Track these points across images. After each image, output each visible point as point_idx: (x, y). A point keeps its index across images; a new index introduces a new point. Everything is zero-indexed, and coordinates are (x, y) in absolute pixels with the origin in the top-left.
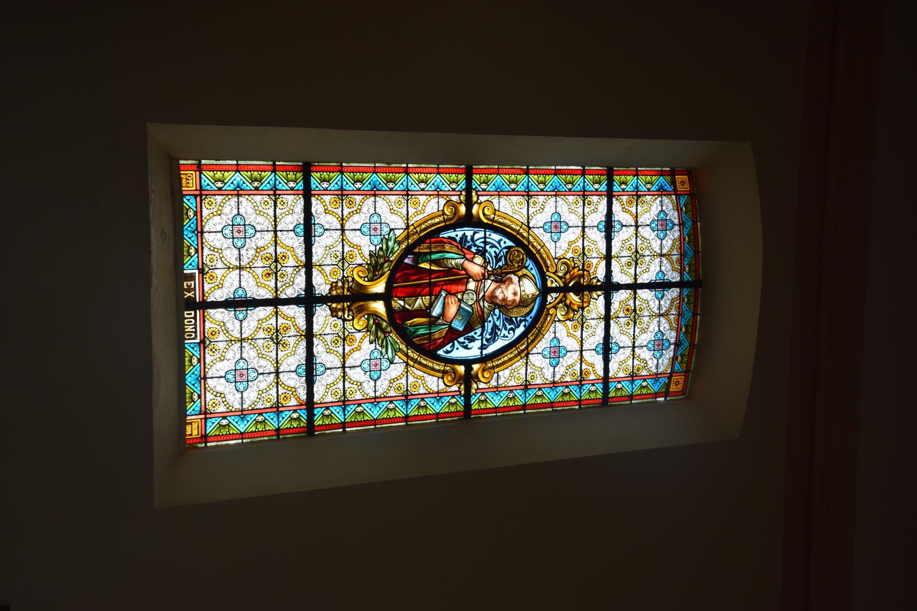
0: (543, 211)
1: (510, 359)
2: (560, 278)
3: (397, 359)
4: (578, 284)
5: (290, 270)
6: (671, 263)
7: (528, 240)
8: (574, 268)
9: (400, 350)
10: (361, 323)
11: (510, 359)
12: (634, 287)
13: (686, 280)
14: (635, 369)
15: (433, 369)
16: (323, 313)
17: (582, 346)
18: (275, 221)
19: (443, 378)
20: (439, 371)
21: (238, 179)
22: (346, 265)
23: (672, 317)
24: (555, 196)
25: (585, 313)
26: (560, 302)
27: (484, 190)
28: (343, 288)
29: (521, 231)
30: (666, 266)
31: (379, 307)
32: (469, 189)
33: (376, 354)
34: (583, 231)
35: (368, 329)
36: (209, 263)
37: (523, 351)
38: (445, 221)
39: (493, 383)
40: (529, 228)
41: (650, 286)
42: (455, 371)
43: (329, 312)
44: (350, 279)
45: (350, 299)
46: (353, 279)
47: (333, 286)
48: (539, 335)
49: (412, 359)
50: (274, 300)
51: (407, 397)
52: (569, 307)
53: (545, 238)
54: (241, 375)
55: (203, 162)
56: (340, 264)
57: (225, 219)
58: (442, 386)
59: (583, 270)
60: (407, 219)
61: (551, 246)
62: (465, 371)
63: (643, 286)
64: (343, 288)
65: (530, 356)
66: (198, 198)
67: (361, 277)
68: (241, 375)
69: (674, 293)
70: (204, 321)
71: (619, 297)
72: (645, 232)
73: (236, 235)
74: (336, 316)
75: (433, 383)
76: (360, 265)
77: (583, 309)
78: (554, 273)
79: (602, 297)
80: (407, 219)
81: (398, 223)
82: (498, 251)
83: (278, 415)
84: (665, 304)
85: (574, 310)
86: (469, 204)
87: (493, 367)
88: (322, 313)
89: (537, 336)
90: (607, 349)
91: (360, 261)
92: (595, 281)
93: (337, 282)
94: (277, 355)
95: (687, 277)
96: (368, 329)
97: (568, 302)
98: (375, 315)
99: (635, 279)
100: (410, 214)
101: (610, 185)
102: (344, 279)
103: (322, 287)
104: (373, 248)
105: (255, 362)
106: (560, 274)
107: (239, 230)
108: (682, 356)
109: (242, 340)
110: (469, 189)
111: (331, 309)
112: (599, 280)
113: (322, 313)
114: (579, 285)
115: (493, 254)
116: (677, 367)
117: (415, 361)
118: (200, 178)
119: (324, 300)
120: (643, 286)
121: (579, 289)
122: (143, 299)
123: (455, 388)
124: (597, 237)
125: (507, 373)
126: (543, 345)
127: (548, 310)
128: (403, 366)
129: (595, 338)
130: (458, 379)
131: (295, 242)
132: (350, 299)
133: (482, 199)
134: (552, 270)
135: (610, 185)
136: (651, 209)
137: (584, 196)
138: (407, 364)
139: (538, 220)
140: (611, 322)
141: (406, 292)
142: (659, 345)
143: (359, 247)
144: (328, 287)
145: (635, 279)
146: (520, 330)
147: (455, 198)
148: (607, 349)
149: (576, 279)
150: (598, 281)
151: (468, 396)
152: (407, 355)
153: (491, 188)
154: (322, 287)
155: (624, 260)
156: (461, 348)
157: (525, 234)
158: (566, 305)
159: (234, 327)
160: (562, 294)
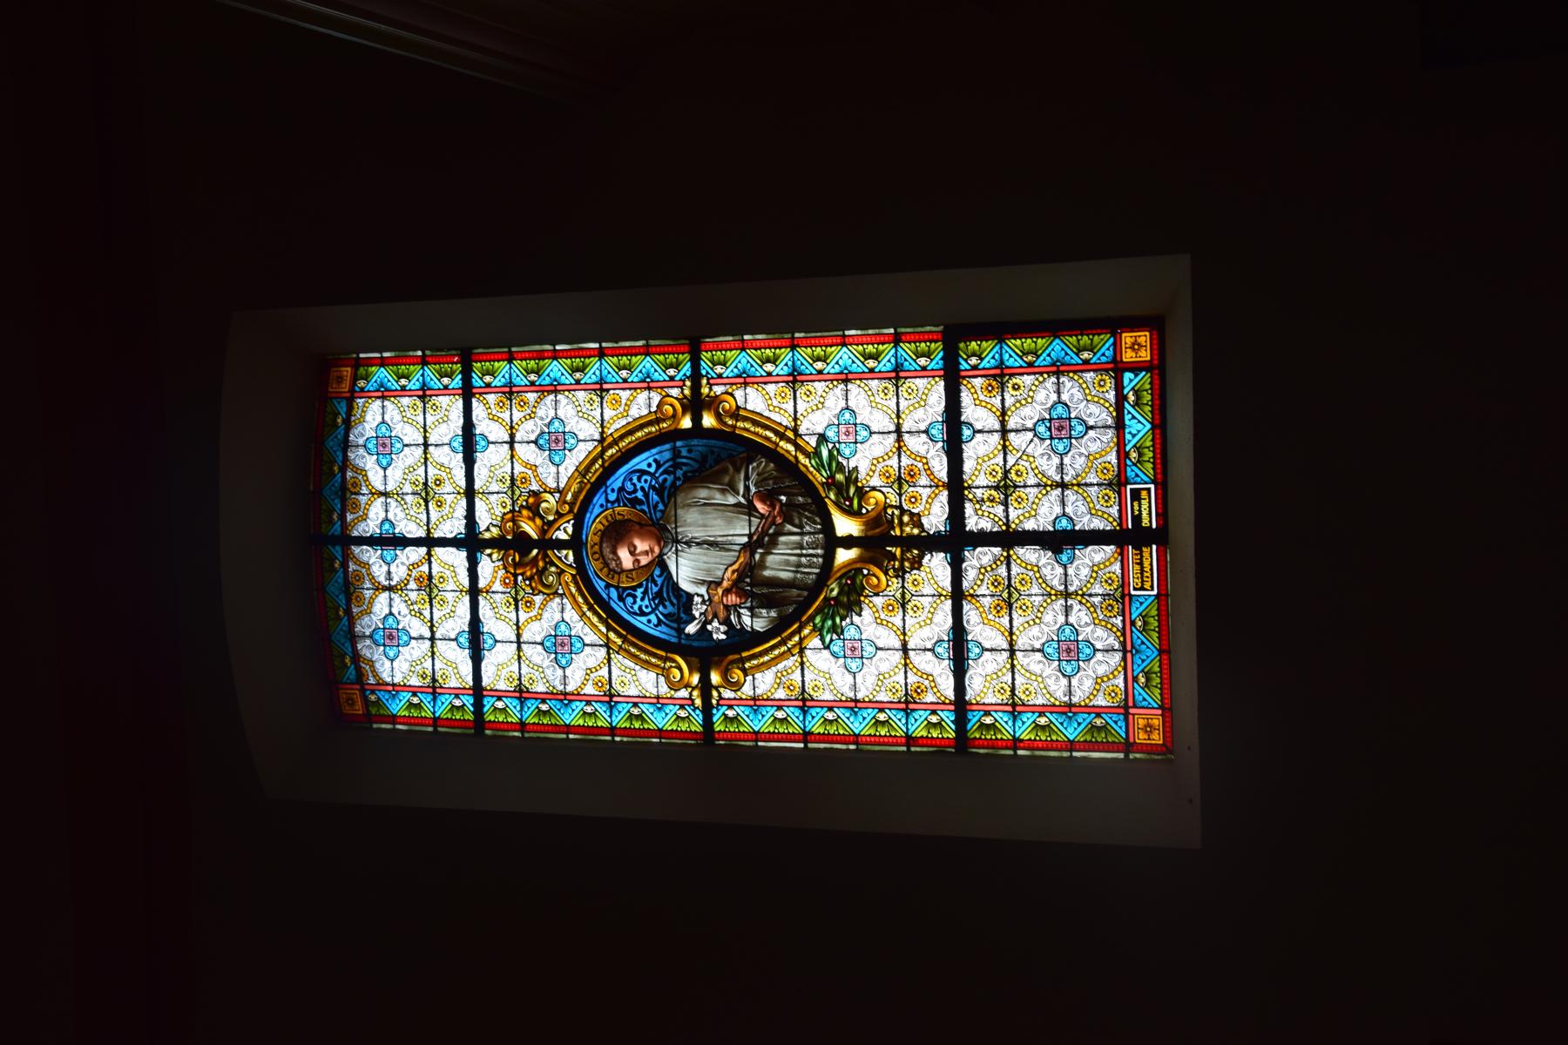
0: (587, 667)
1: (631, 432)
2: (553, 564)
3: (813, 441)
4: (524, 552)
5: (926, 601)
6: (372, 579)
7: (609, 628)
8: (531, 578)
9: (807, 455)
10: (872, 501)
11: (631, 432)
12: (429, 542)
13: (338, 548)
14: (420, 410)
15: (755, 423)
16: (934, 521)
18: (1013, 666)
19: (738, 408)
20: (745, 419)
21: (1071, 730)
22: (898, 595)
23: (364, 490)
24: (566, 694)
25: (509, 502)
26: (550, 524)
27: (682, 707)
28: (902, 561)
29: (619, 641)
30: (379, 571)
31: (845, 526)
32: (707, 710)
33: (847, 451)
34: (519, 636)
35: (862, 493)
37: (610, 446)
38: (743, 660)
40: (607, 646)
41: (402, 542)
42: (718, 417)
43: (924, 521)
44: (891, 573)
46: (886, 574)
47: (917, 564)
48: (582, 471)
49: (789, 440)
50: (987, 552)
51: (795, 379)
52: (535, 510)
53: (579, 628)
54: (1055, 429)
55: (1121, 756)
56: (908, 596)
58: (739, 394)
59: (515, 575)
60: (802, 664)
61: (571, 615)
62: (701, 418)
63: (417, 542)
64: (902, 561)
65: (597, 436)
68: (1055, 429)
69: (371, 527)
70: (1120, 517)
71: (453, 526)
74: (912, 515)
75: (754, 400)
76: (877, 594)
77: (512, 511)
79: (483, 527)
80: (802, 664)
83: (1002, 362)
84: (376, 511)
85: (528, 507)
86: (706, 687)
87: (658, 421)
89: (587, 469)
90: (469, 443)
91: (878, 601)
92: (495, 556)
95: (337, 551)
96: (862, 493)
97: (538, 521)
98: (849, 512)
99: (429, 554)
100: (799, 671)
101: (478, 705)
102: (901, 573)
103: (937, 565)
104: (856, 619)
105: (1039, 449)
106: (553, 569)
108: (335, 425)
110: (707, 710)
111: (920, 525)
113: (936, 518)
116: (342, 408)
117: (782, 436)
118: (1127, 732)
119: (931, 543)
120: (417, 542)
122: (1233, 549)
123: (718, 390)
124: (496, 624)
125: (635, 412)
126: (579, 454)
127: (571, 511)
128: (802, 430)
129: (491, 461)
130: (713, 403)
131: (982, 630)
132: (892, 544)
133: (684, 693)
134: (568, 578)
135: (478, 705)
137: (521, 691)
138: (795, 430)
141: (827, 546)
142: (385, 446)
143: (879, 622)
145: (429, 554)
146: (616, 481)
147: (727, 694)
148: (469, 443)
149: (527, 559)
150: (490, 555)
151: (696, 376)
152: (798, 447)
153: (672, 709)
154: (937, 565)
155: (451, 586)
156: (644, 466)
157: (612, 635)
158: (542, 518)
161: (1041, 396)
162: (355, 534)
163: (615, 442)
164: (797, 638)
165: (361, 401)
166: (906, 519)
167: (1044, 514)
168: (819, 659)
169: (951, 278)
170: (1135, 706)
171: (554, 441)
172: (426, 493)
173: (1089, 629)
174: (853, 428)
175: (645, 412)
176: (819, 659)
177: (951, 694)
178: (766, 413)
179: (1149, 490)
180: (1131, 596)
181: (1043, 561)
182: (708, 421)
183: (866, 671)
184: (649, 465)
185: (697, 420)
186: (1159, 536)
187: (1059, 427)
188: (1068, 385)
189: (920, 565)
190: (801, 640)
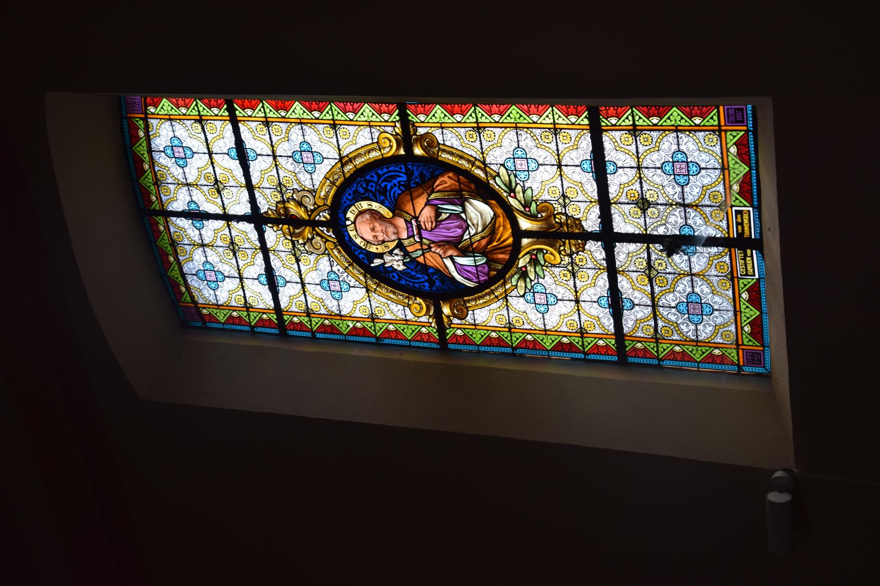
31: (525, 224)
37: (347, 163)
40: (366, 287)
43: (584, 223)
45: (560, 233)
46: (560, 253)
49: (478, 167)
52: (300, 204)
53: (323, 169)
63: (216, 217)
66: (740, 343)
67: (552, 254)
68: (680, 166)
69: (179, 205)
72: (655, 177)
75: (450, 139)
78: (327, 240)
81: (518, 304)
95: (161, 220)
112: (624, 229)
119: (588, 236)
120: (216, 217)
124: (283, 268)
136: (226, 293)
139: (360, 293)
140: (256, 192)
152: (486, 173)
159: (193, 234)
160: (312, 218)
161: (665, 146)
163: (350, 161)
167: (672, 223)
169: (596, 78)
171: (305, 155)
172: (218, 187)
173: (709, 296)
176: (518, 304)
177: (612, 329)
178: (460, 148)
179: (749, 211)
181: (581, 151)
183: (556, 304)
185: (409, 149)
186: (757, 244)
189: (584, 250)
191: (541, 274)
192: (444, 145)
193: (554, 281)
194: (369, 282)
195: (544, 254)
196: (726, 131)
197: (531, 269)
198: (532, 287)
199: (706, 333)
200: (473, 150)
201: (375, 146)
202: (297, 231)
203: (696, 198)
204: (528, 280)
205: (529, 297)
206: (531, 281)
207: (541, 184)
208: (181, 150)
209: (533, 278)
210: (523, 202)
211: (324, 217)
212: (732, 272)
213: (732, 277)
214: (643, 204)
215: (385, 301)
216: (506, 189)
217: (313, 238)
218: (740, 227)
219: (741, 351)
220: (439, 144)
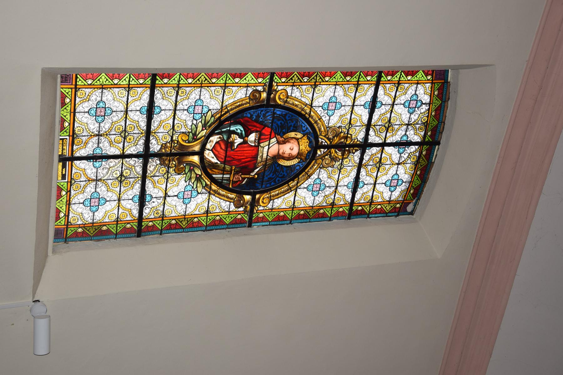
12: (383, 145)
15: (228, 197)
17: (354, 102)
36: (72, 221)
37: (293, 186)
39: (270, 206)
43: (158, 162)
46: (178, 141)
47: (164, 146)
57: (92, 103)
61: (325, 119)
65: (298, 190)
73: (414, 106)
75: (225, 205)
78: (325, 136)
82: (283, 123)
88: (154, 164)
90: (373, 105)
92: (356, 140)
93: (166, 144)
94: (128, 99)
103: (155, 147)
107: (101, 112)
109: (99, 135)
113: (154, 164)
114: (345, 147)
115: (279, 124)
119: (157, 155)
121: (341, 147)
125: (280, 200)
129: (348, 178)
139: (319, 101)
144: (160, 147)
145: (385, 140)
147: (260, 88)
148: (373, 105)
154: (155, 147)
162: (417, 147)
164: (223, 113)
165: (400, 199)
166: (167, 162)
168: (215, 105)
170: (72, 88)
171: (316, 190)
173: (110, 121)
174: (185, 199)
175: (275, 200)
180: (69, 136)
182: (248, 198)
184: (279, 180)
185: (254, 198)
187: (96, 201)
188: (296, 90)
189: (162, 146)
190: (221, 112)
191: (193, 126)
192: (230, 202)
193: (185, 121)
194: (308, 111)
195: (188, 140)
196: (64, 225)
197: (200, 128)
198: (202, 117)
199: (96, 95)
200: (215, 199)
201: (272, 198)
202: (343, 140)
203: (94, 93)
204: (203, 122)
205: (205, 110)
206: (201, 122)
207: (179, 183)
208: (395, 184)
209: (200, 124)
210: (193, 172)
211: (321, 151)
212: (76, 91)
213: (73, 136)
214: (124, 134)
215: (303, 99)
216: (202, 181)
217: (334, 137)
218: (64, 173)
219: (74, 83)
220: (233, 202)
